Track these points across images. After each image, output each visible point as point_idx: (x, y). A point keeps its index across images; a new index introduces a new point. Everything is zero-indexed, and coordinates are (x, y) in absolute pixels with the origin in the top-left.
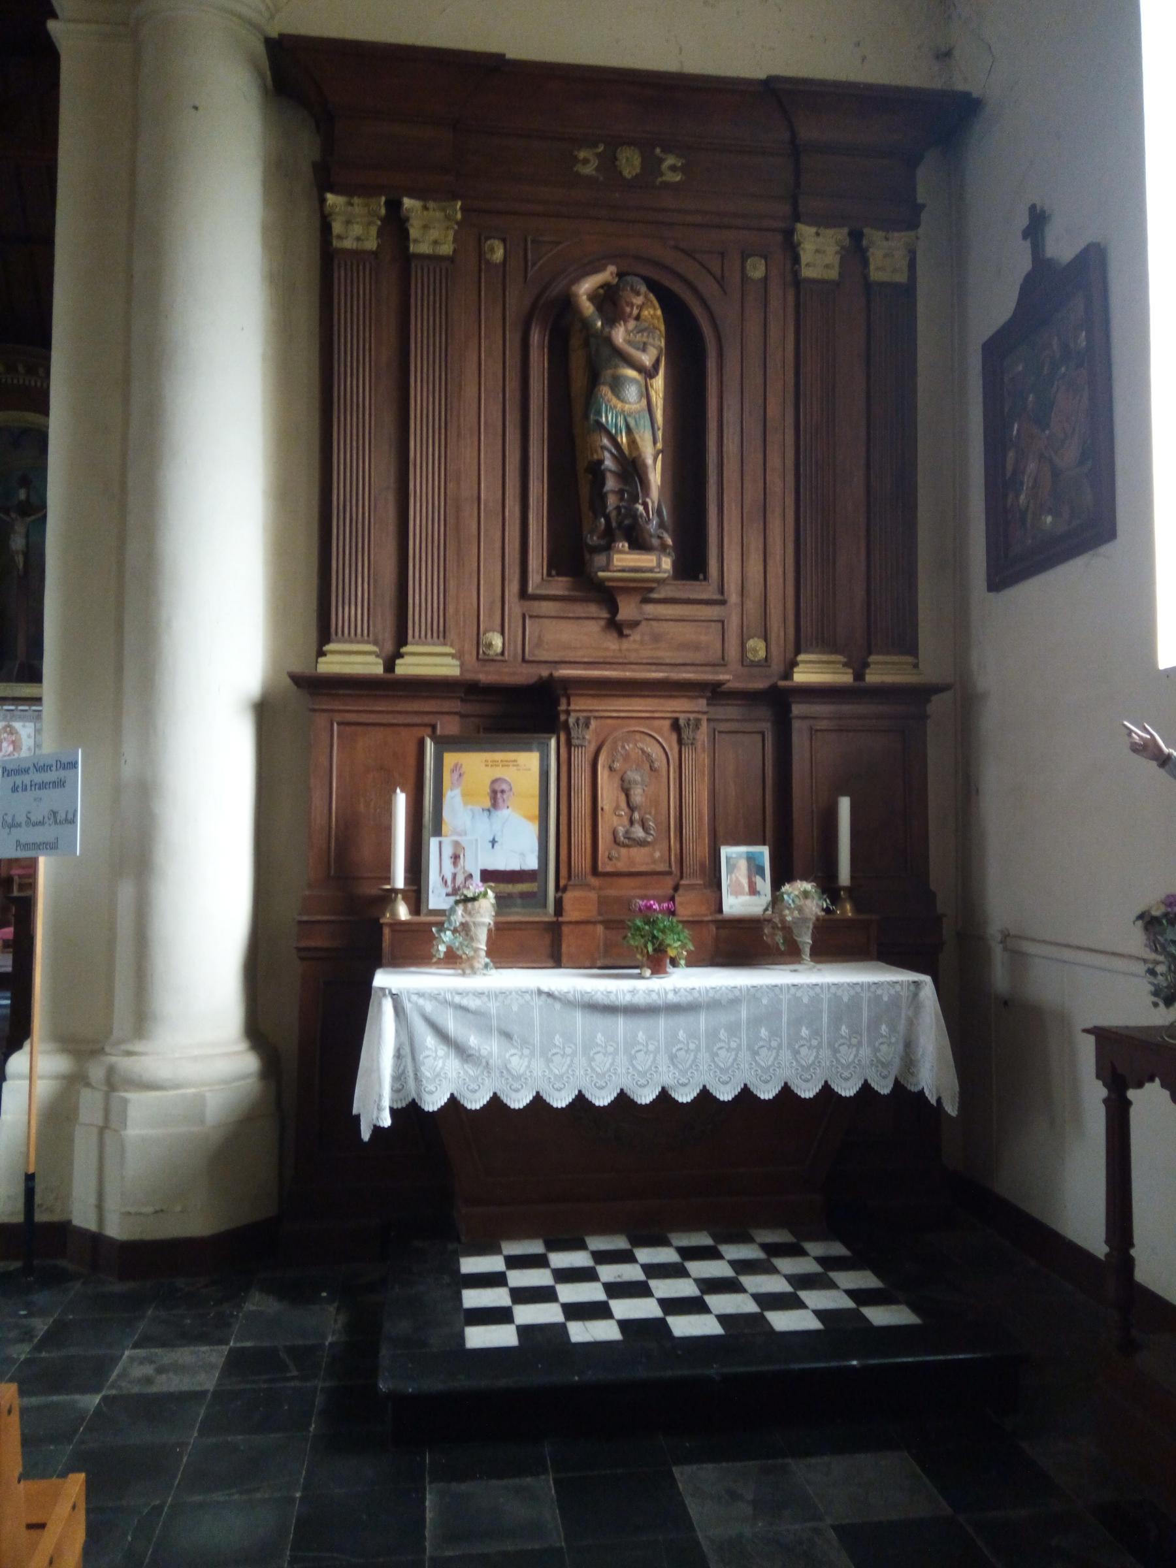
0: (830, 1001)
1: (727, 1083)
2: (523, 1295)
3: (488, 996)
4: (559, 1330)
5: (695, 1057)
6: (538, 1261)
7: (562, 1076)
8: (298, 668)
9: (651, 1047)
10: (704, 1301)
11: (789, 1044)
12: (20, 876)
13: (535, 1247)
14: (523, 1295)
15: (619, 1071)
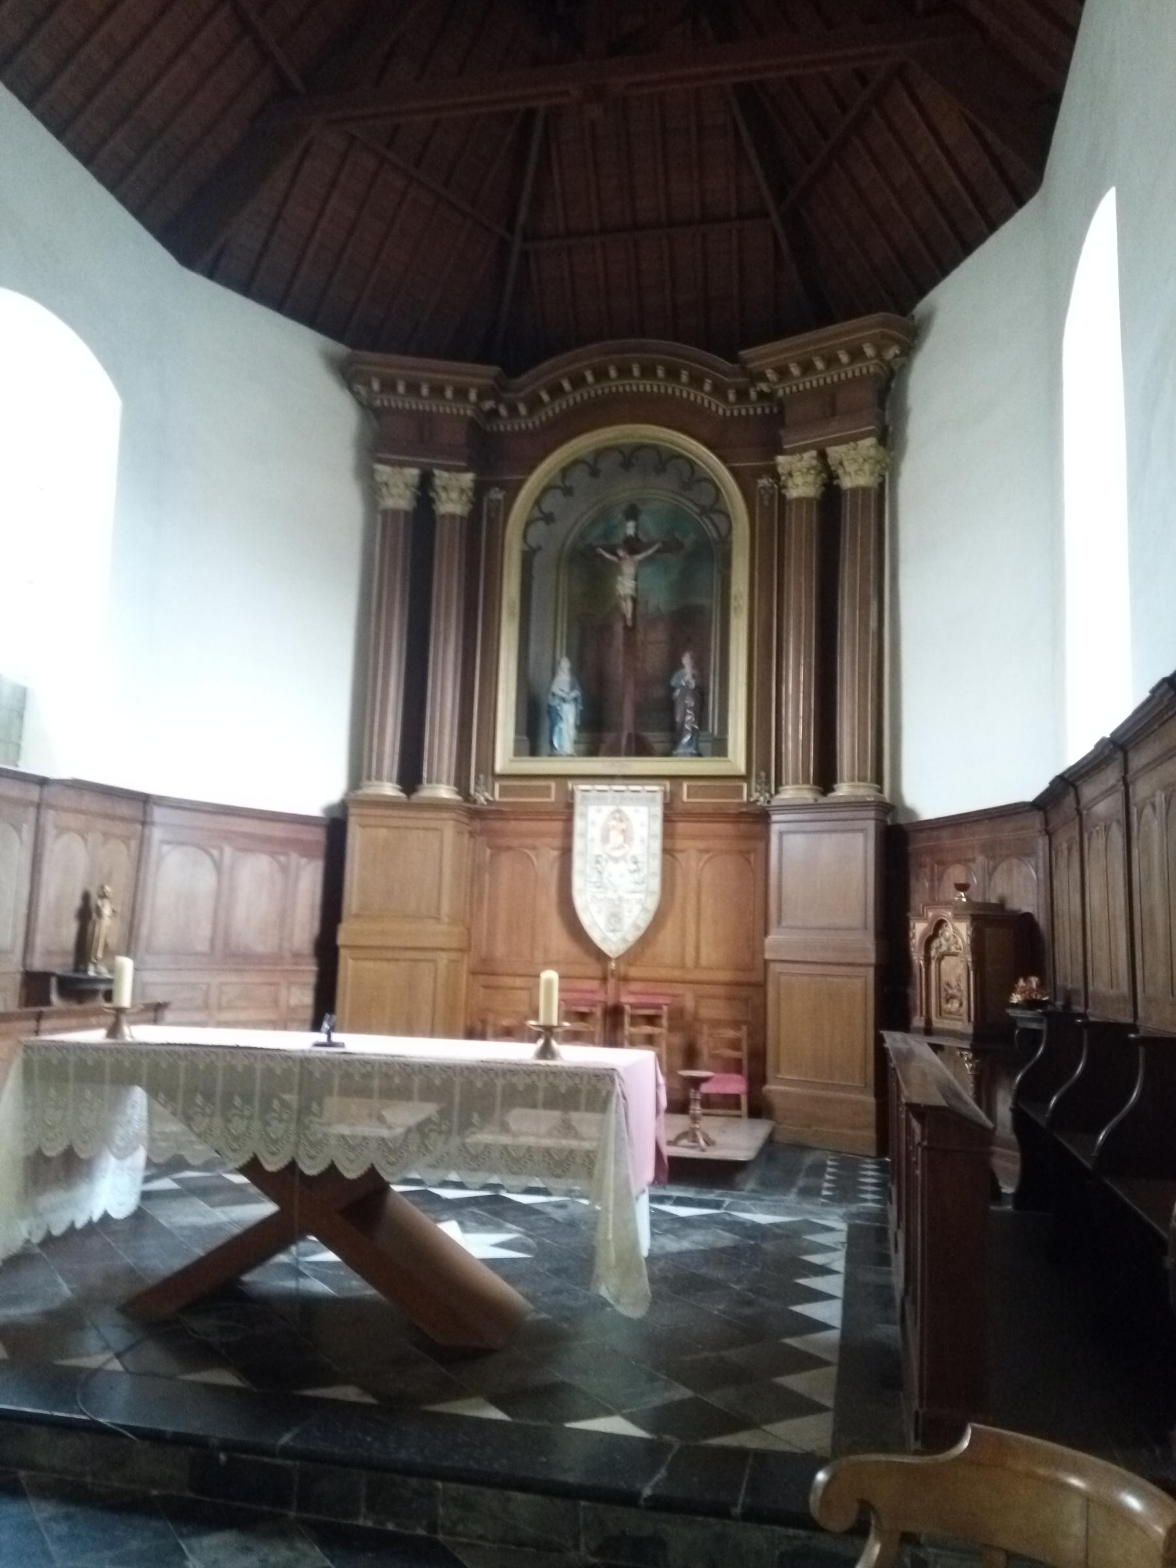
3: (581, 1078)
9: (444, 1128)
12: (633, 1006)
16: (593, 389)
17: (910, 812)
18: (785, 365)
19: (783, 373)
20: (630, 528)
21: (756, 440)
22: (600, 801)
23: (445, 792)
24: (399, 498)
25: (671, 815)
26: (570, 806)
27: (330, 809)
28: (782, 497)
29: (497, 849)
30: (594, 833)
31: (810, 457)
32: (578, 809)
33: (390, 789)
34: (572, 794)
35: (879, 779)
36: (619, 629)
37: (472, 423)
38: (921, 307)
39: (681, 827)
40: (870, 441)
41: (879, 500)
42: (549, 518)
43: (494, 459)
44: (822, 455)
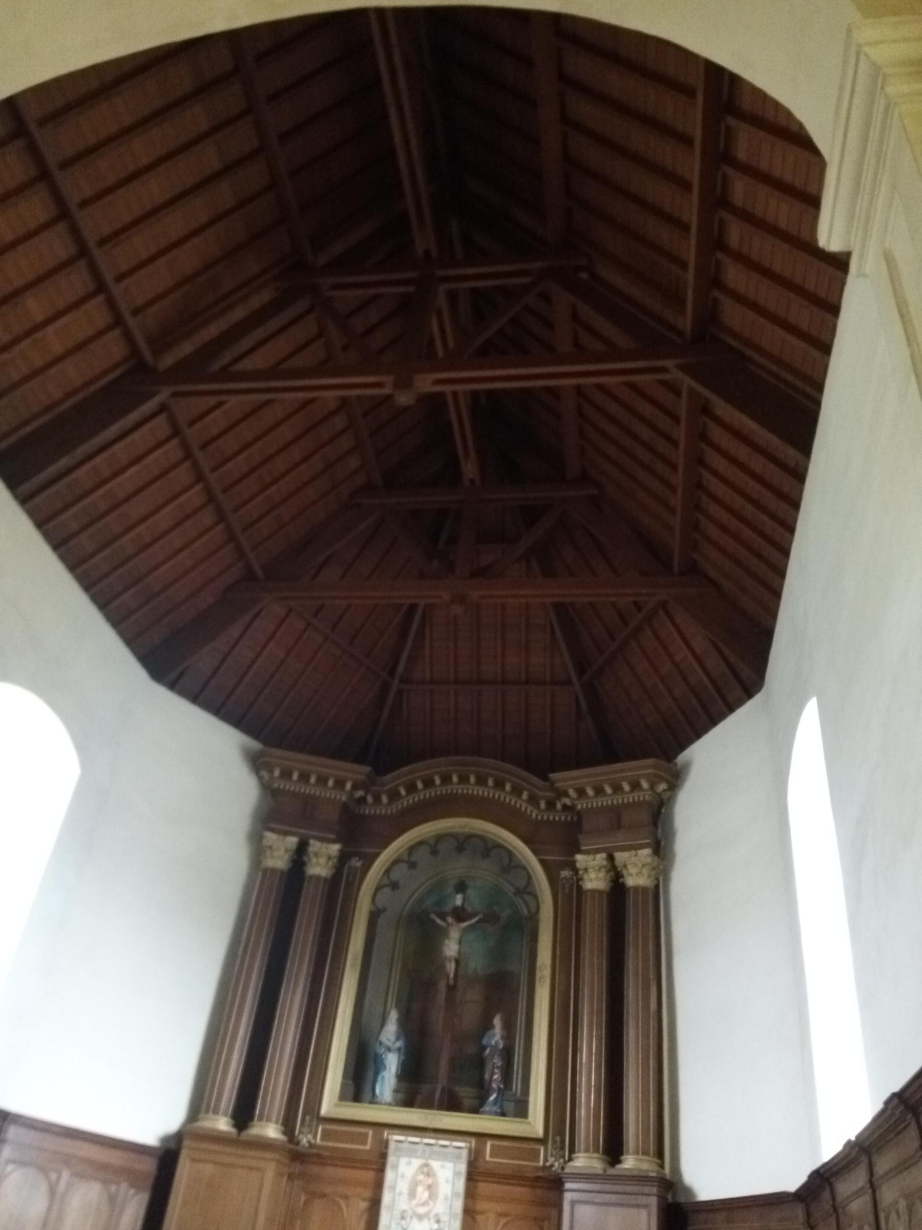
16: (439, 789)
17: (689, 1191)
18: (584, 787)
19: (581, 792)
20: (459, 900)
21: (562, 839)
22: (412, 1154)
23: (272, 1131)
24: (279, 860)
25: (475, 1174)
26: (383, 1156)
27: (166, 1139)
28: (580, 888)
29: (312, 1195)
30: (403, 1186)
31: (601, 858)
32: (391, 1160)
33: (223, 1124)
34: (386, 1143)
35: (660, 1154)
36: (442, 986)
37: (345, 807)
38: (682, 758)
39: (483, 1187)
40: (647, 851)
41: (656, 898)
42: (394, 886)
43: (358, 834)
44: (611, 858)
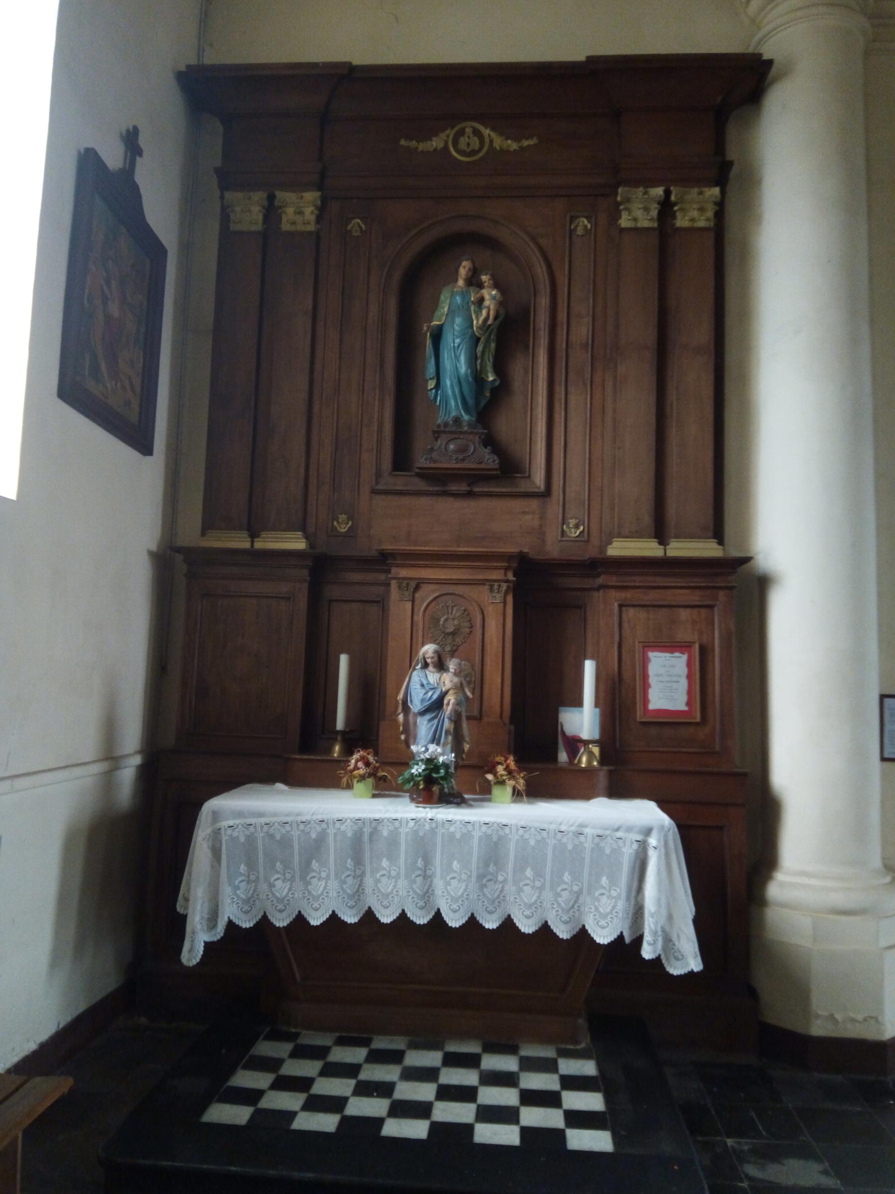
0: (480, 838)
1: (283, 911)
2: (531, 1098)
4: (558, 1135)
5: (503, 887)
6: (549, 1066)
7: (283, 899)
8: (752, 562)
10: (346, 1116)
11: (336, 874)
13: (548, 1052)
14: (531, 1098)
15: (331, 894)
